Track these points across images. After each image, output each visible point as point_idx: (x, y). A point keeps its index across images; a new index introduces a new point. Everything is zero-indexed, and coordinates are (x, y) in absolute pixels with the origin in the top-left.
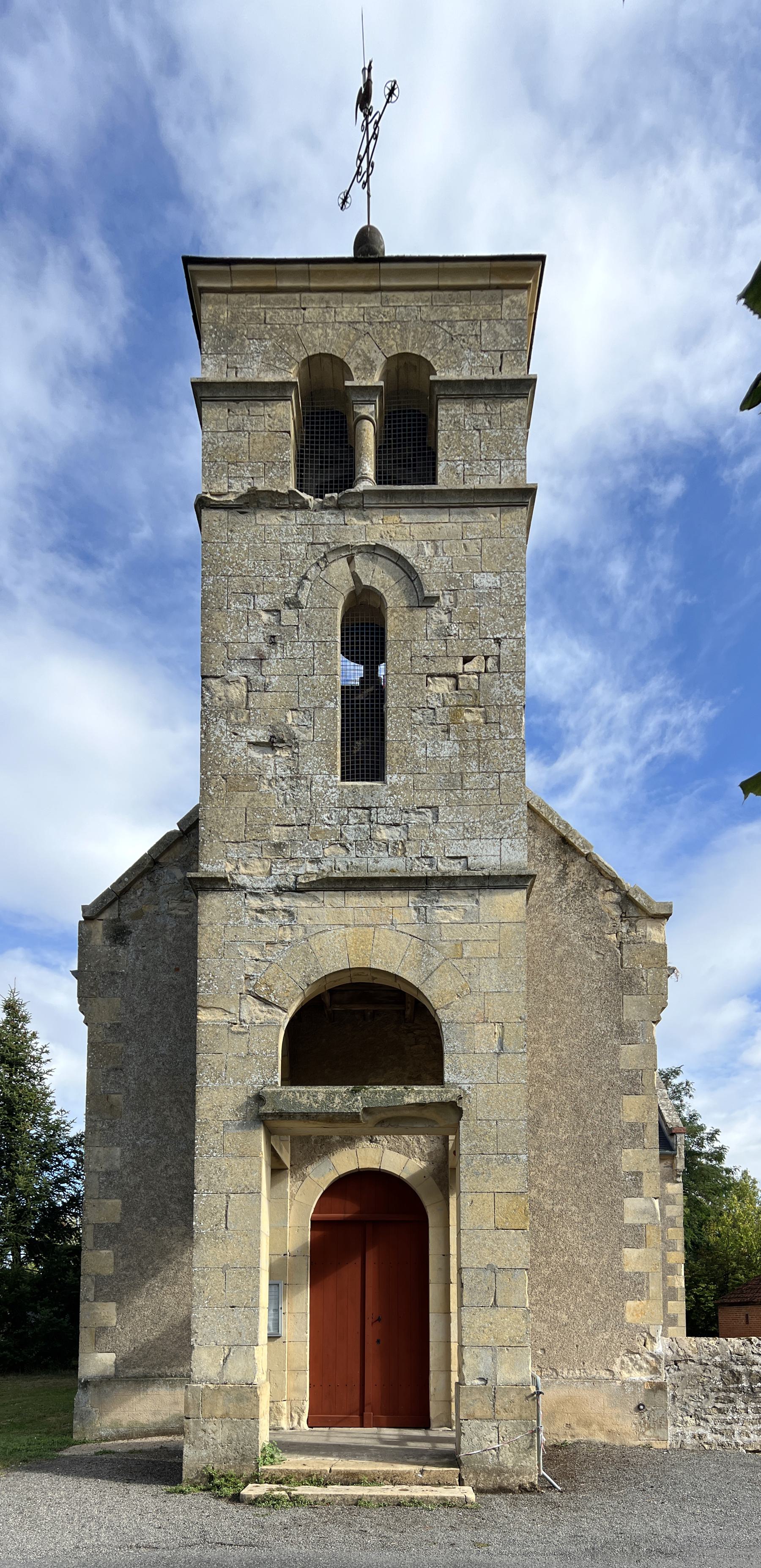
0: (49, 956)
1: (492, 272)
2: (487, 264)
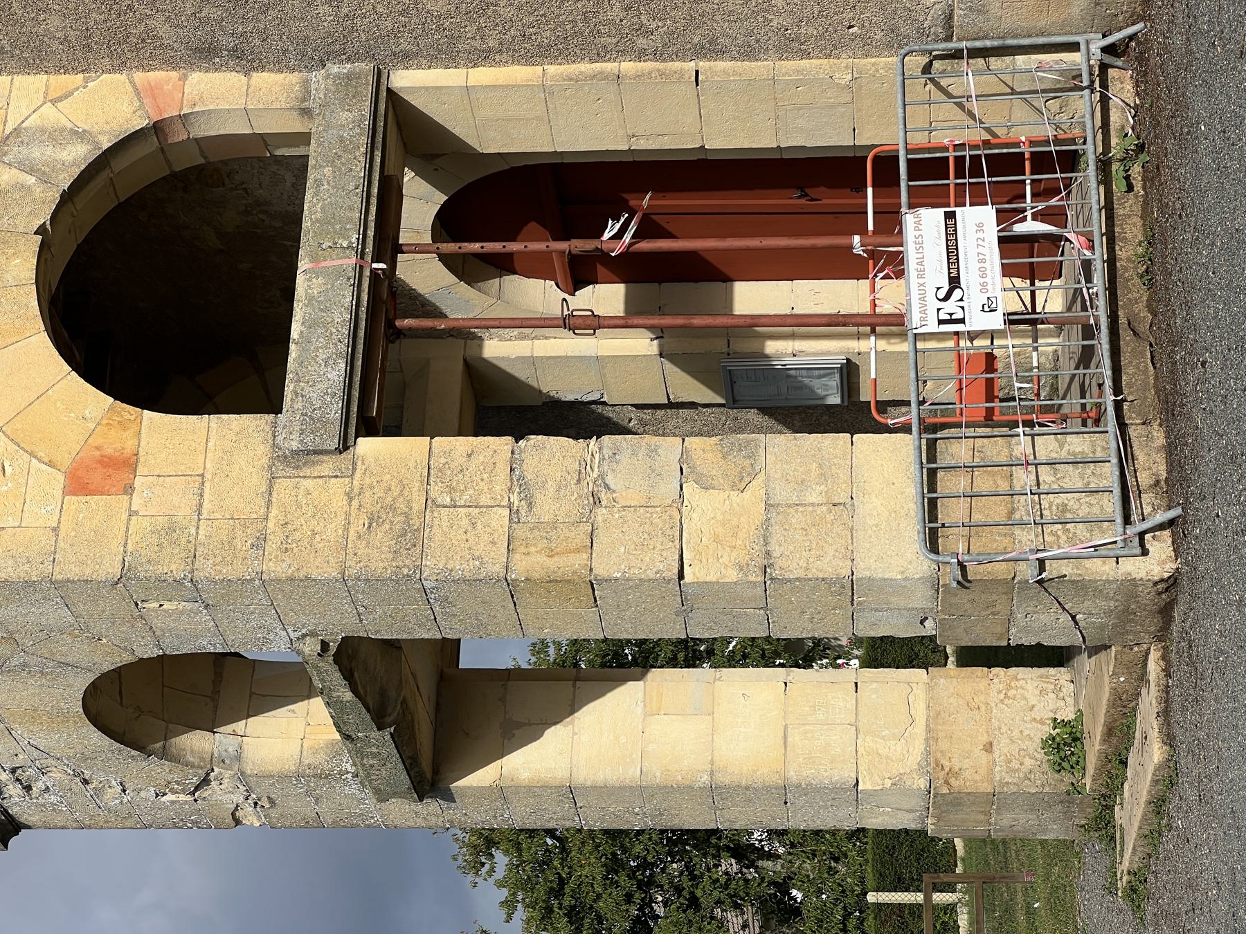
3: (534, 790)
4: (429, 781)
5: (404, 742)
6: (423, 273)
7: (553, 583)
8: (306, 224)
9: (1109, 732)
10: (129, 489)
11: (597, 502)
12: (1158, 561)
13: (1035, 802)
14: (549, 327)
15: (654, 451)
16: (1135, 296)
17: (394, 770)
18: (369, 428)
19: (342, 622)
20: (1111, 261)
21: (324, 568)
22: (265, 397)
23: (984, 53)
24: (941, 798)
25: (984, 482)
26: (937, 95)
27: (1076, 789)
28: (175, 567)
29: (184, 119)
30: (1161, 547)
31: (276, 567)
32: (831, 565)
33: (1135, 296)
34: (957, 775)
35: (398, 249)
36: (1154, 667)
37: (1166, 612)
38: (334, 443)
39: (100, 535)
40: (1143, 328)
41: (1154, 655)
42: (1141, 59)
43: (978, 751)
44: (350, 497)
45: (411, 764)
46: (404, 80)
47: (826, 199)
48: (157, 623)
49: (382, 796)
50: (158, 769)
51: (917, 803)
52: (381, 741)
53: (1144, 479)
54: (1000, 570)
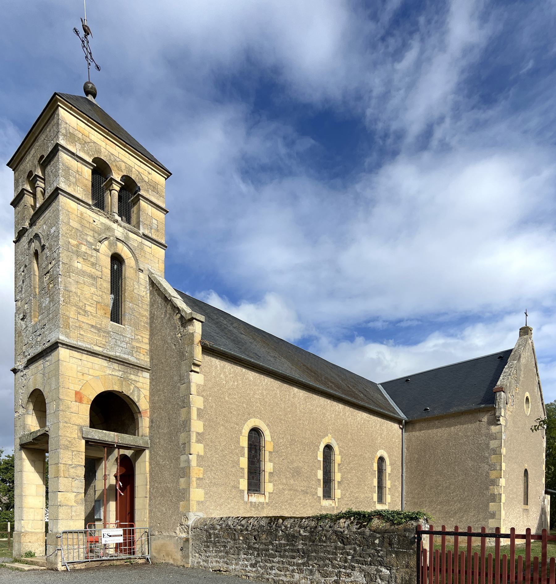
0: (452, 331)
1: (50, 109)
2: (48, 108)
3: (22, 465)
4: (23, 447)
5: (30, 443)
6: (116, 453)
7: (58, 471)
8: (123, 434)
9: (32, 561)
10: (76, 401)
11: (73, 479)
12: (60, 568)
13: (19, 550)
14: (109, 472)
15: (82, 488)
16: (108, 564)
17: (25, 441)
18: (87, 442)
19: (51, 435)
20: (113, 560)
21: (61, 433)
22: (93, 425)
23: (148, 541)
24: (20, 534)
25: (75, 541)
26: (142, 534)
27: (22, 556)
28: (61, 408)
29: (141, 417)
30: (63, 568)
31: (61, 425)
32: (61, 516)
33: (108, 564)
34: (25, 537)
35: (119, 449)
36: (42, 568)
37: (52, 569)
38: (84, 436)
39: (67, 396)
40: (102, 565)
41: (45, 568)
42: (146, 564)
43: (29, 540)
44: (74, 438)
45: (26, 444)
46: (147, 452)
47: (127, 516)
48: (52, 403)
49: (20, 438)
50: (26, 400)
51: (19, 530)
52: (30, 439)
53: (76, 566)
54: (59, 543)
